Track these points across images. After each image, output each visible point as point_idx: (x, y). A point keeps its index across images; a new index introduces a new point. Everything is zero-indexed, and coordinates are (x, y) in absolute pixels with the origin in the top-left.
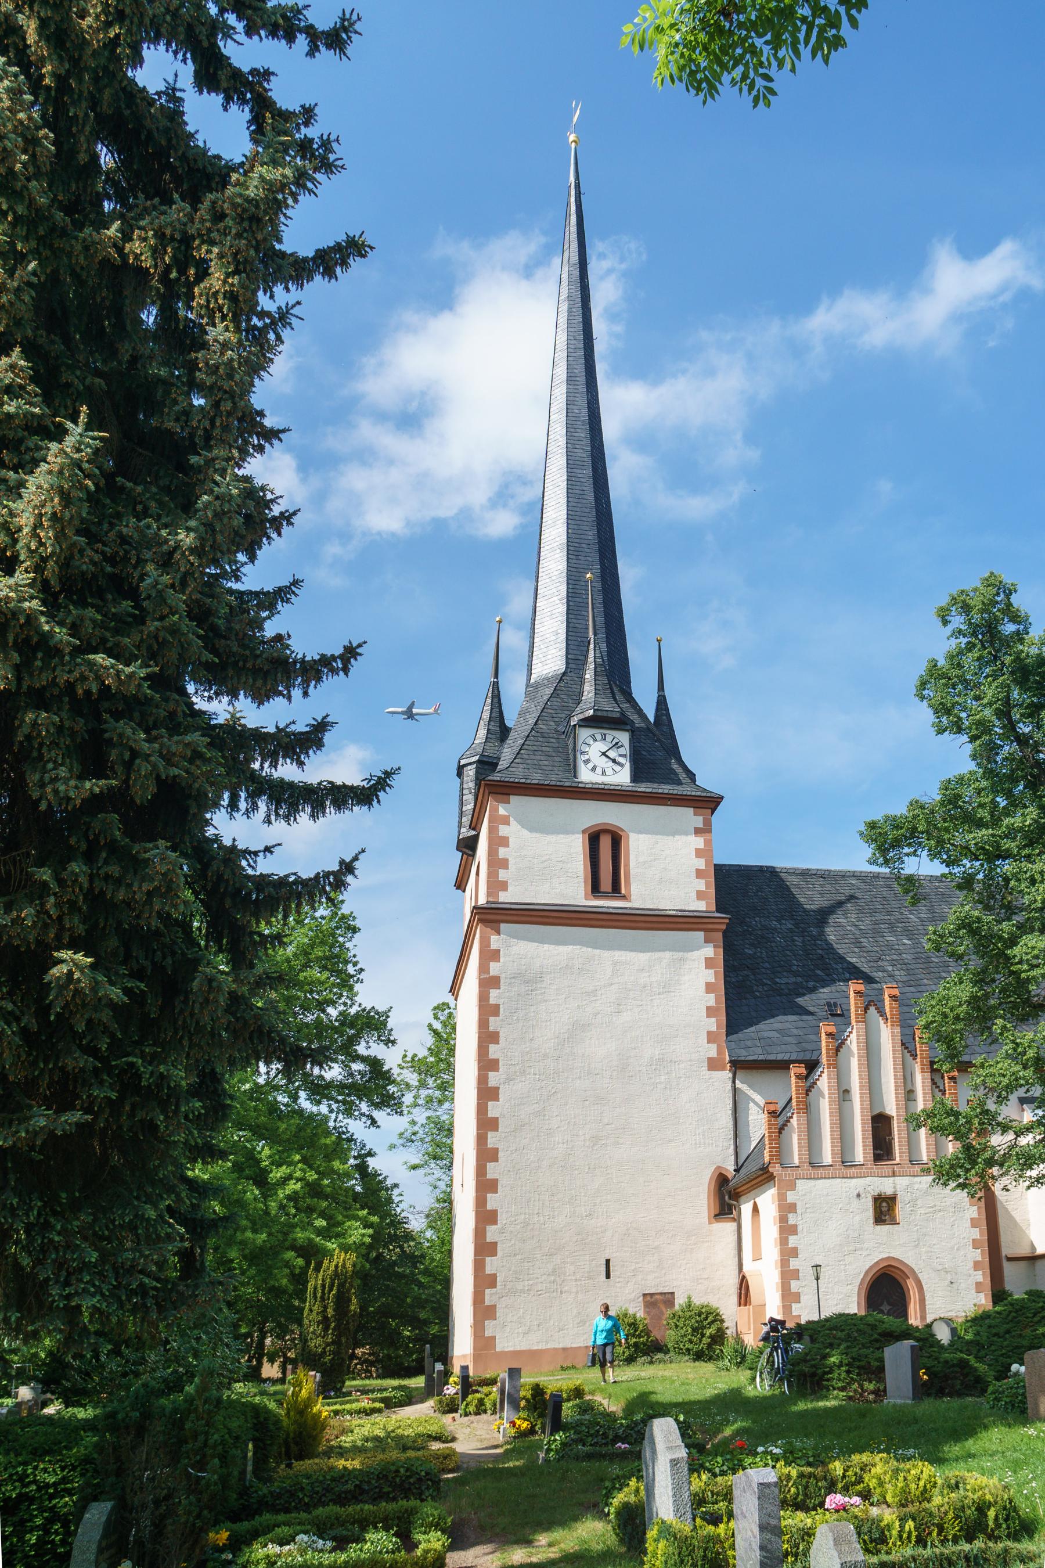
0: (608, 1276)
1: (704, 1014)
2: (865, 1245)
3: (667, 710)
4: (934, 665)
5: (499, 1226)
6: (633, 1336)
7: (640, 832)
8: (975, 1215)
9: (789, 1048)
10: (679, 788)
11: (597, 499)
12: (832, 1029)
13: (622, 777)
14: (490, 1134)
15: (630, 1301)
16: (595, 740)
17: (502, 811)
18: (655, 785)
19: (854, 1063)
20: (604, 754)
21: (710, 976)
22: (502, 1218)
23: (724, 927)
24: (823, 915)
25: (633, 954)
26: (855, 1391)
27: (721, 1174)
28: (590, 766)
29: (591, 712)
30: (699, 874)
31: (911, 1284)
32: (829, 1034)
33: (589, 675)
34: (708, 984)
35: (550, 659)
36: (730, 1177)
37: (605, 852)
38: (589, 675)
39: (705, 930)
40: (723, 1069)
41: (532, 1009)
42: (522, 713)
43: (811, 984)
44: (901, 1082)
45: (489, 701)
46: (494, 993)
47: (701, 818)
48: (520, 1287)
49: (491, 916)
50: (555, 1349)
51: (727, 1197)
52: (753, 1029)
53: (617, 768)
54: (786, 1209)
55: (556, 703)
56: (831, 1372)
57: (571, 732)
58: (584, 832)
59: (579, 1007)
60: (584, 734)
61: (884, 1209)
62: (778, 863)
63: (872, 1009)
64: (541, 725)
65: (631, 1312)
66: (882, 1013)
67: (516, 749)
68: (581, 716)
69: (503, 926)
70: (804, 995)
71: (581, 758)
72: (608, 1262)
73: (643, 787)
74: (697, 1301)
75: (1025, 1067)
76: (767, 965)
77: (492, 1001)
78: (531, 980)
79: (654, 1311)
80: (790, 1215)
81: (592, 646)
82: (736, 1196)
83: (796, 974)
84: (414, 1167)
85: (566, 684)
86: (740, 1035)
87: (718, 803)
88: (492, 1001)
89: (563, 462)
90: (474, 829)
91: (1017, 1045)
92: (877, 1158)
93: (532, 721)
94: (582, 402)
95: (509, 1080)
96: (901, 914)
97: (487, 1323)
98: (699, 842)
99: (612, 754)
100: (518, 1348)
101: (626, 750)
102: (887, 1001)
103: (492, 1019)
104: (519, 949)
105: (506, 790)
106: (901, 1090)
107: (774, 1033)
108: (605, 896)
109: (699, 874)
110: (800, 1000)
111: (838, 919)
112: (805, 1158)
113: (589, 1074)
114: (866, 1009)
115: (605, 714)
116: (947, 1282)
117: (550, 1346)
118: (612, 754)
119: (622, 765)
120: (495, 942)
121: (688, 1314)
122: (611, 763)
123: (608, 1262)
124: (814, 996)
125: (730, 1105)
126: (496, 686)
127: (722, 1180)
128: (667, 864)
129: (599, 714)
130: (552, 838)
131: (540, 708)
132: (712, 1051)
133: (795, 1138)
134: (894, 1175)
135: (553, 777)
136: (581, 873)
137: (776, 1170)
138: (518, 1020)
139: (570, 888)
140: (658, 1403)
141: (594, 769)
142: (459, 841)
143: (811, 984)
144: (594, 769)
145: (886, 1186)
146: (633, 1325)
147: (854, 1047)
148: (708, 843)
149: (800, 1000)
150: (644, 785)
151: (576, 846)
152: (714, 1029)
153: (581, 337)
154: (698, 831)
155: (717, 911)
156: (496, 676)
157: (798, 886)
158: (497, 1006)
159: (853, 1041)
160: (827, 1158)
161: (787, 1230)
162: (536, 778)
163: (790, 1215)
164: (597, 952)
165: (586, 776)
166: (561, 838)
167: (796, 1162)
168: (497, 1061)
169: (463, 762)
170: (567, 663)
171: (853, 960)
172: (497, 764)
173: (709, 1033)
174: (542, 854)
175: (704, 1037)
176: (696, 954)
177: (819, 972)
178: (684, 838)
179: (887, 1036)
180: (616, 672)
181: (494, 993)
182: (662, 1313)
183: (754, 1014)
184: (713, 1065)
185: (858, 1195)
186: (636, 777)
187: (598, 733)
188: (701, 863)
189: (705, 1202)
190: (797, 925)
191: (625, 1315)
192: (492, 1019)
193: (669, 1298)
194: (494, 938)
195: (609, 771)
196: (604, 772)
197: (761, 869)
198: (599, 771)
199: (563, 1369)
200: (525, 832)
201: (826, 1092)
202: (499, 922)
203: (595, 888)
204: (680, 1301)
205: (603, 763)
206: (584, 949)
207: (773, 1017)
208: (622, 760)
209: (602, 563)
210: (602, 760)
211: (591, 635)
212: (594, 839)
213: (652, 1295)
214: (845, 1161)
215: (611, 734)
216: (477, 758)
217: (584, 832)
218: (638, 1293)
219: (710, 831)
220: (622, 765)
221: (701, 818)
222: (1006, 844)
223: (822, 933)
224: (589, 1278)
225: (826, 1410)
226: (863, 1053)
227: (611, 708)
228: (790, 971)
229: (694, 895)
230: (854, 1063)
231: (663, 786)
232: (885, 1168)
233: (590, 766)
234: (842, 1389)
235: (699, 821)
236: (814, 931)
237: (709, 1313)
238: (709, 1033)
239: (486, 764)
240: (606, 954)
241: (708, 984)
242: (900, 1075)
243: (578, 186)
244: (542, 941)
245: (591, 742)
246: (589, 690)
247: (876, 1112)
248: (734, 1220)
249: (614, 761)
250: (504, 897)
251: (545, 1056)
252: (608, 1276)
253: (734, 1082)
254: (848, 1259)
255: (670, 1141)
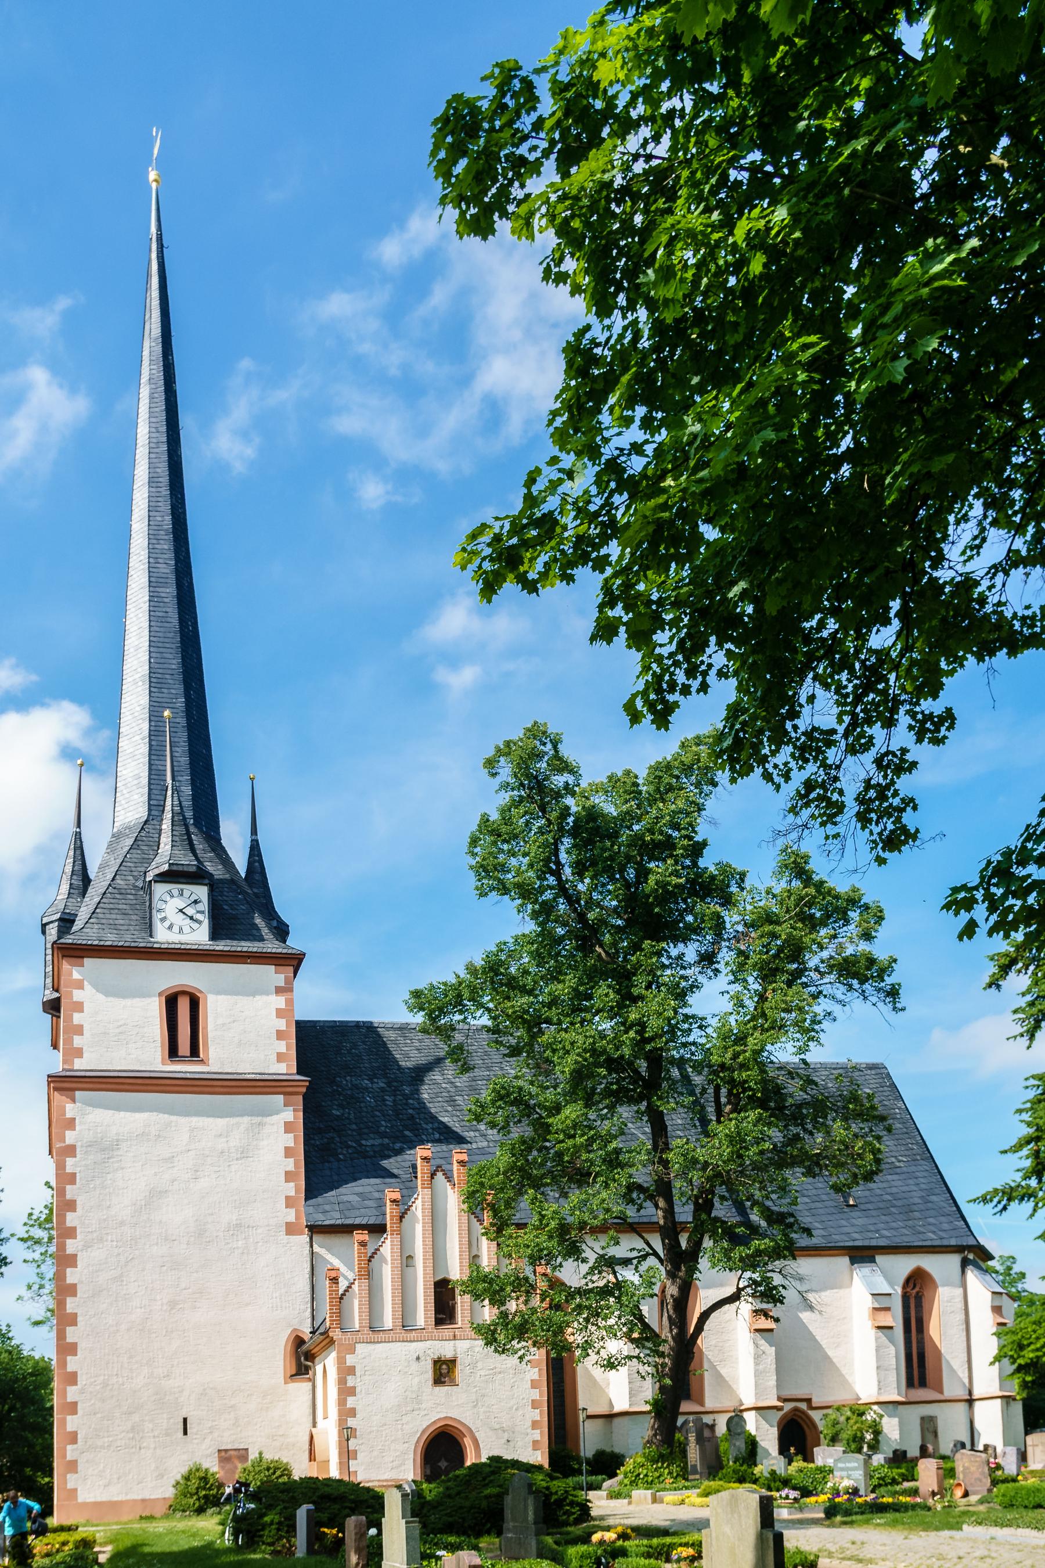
0: (185, 1433)
1: (283, 1179)
2: (423, 1406)
3: (260, 855)
4: (485, 820)
5: (79, 1386)
6: (204, 1489)
7: (218, 993)
8: (536, 1377)
9: (368, 1212)
10: (260, 944)
11: (182, 621)
12: (397, 1196)
13: (199, 935)
14: (69, 1300)
15: (207, 1456)
16: (172, 896)
17: (76, 975)
18: (235, 943)
19: (419, 1228)
20: (181, 911)
21: (289, 1140)
22: (82, 1380)
23: (304, 1090)
24: (420, 1073)
25: (211, 1120)
26: (283, 1546)
27: (297, 1337)
28: (167, 924)
29: (166, 867)
30: (280, 1035)
31: (467, 1442)
32: (393, 1201)
33: (166, 825)
34: (287, 1149)
35: (133, 808)
36: (306, 1339)
37: (182, 1013)
38: (166, 825)
39: (284, 1094)
40: (302, 1234)
41: (109, 1176)
42: (102, 867)
43: (398, 1146)
44: (466, 1247)
45: (72, 853)
46: (70, 1162)
47: (282, 976)
48: (99, 1443)
49: (64, 1084)
50: (135, 1501)
51: (303, 1358)
52: (333, 1193)
53: (195, 925)
54: (346, 1371)
55: (136, 854)
56: (263, 1529)
57: (148, 888)
58: (160, 994)
59: (156, 1174)
60: (160, 890)
61: (444, 1371)
62: (376, 1019)
63: (440, 1174)
64: (119, 881)
65: (205, 1466)
66: (449, 1178)
67: (92, 908)
68: (157, 871)
69: (78, 1093)
70: (389, 1157)
71: (157, 917)
72: (185, 1420)
73: (221, 946)
74: (268, 1456)
75: (551, 1237)
76: (354, 1127)
77: (69, 1170)
78: (107, 1148)
79: (228, 1466)
80: (349, 1378)
81: (169, 793)
82: (310, 1356)
83: (383, 1135)
84: (37, 1323)
85: (145, 837)
86: (320, 1200)
87: (300, 961)
88: (69, 1170)
89: (145, 580)
90: (57, 991)
91: (543, 1216)
92: (439, 1322)
93: (110, 876)
94: (165, 507)
95: (87, 1247)
96: (502, 1069)
97: (69, 1476)
98: (280, 1002)
99: (190, 911)
100: (99, 1499)
101: (204, 906)
102: (455, 1166)
103: (68, 1187)
104: (93, 1117)
105: (77, 952)
106: (466, 1255)
107: (351, 1197)
108: (183, 1060)
109: (280, 1035)
110: (385, 1163)
111: (436, 1076)
112: (366, 1323)
113: (166, 1239)
114: (433, 1175)
115: (180, 868)
116: (504, 1441)
117: (129, 1497)
118: (190, 911)
119: (200, 922)
120: (71, 1110)
121: (257, 1469)
122: (188, 921)
123: (185, 1420)
124: (399, 1158)
125: (309, 1269)
126: (78, 836)
127: (299, 1342)
128: (250, 1023)
129: (175, 868)
130: (129, 1002)
131: (119, 861)
132: (291, 1216)
133: (356, 1302)
134: (455, 1338)
135: (128, 937)
136: (158, 1038)
137: (336, 1334)
138: (95, 1188)
139: (147, 1053)
140: (151, 1554)
141: (170, 927)
142: (44, 1003)
143: (398, 1146)
144: (170, 927)
145: (446, 1350)
146: (204, 1479)
147: (419, 1214)
148: (290, 1002)
149: (385, 1163)
150: (223, 942)
151: (154, 1010)
152: (293, 1194)
153: (164, 429)
154: (279, 991)
155: (298, 1073)
156: (79, 825)
157: (395, 1042)
158: (74, 1175)
159: (419, 1207)
160: (388, 1322)
161: (346, 1391)
162: (110, 939)
163: (349, 1378)
164: (174, 1118)
165: (163, 936)
166: (137, 1002)
167: (357, 1326)
168: (74, 1229)
169: (45, 920)
170: (150, 810)
171: (445, 1120)
172: (73, 921)
173: (287, 1198)
174: (118, 1017)
175: (282, 1202)
176: (275, 1118)
177: (407, 1133)
178: (265, 998)
179: (453, 1201)
180: (202, 816)
181: (70, 1162)
182: (236, 1468)
183: (335, 1178)
184: (291, 1229)
185: (418, 1358)
186: (214, 935)
187: (175, 888)
188: (282, 1024)
189: (282, 1363)
190: (389, 1084)
191: (198, 1470)
192: (68, 1187)
193: (242, 1454)
194: (69, 1106)
195: (186, 929)
196: (181, 930)
197: (358, 1025)
198: (176, 929)
199: (141, 1518)
200: (101, 997)
201: (389, 1259)
202: (74, 1090)
203: (173, 1052)
204: (253, 1455)
205: (179, 920)
206: (161, 1115)
207: (355, 1180)
208: (199, 917)
209: (187, 696)
210: (181, 917)
211: (169, 781)
212: (171, 1002)
213: (226, 1451)
214: (405, 1324)
215: (188, 889)
216: (58, 916)
217: (160, 994)
218: (213, 1450)
219: (291, 990)
220: (200, 922)
221: (282, 976)
222: (546, 1013)
223: (417, 1091)
224: (167, 1435)
225: (255, 1561)
226: (428, 1220)
227: (187, 860)
228: (377, 1133)
229: (274, 1057)
230: (419, 1228)
231: (243, 943)
232: (446, 1331)
233: (167, 924)
234: (272, 1544)
235: (280, 979)
236: (407, 1090)
237: (276, 1469)
238: (287, 1198)
239: (66, 922)
240: (182, 1120)
241: (287, 1149)
242: (465, 1240)
243: (160, 238)
244: (118, 1108)
245: (168, 898)
246: (166, 840)
247: (438, 1278)
248: (309, 1380)
249: (191, 918)
250: (80, 1065)
251: (122, 1223)
252: (185, 1433)
253: (312, 1246)
254: (405, 1419)
255: (247, 1304)
